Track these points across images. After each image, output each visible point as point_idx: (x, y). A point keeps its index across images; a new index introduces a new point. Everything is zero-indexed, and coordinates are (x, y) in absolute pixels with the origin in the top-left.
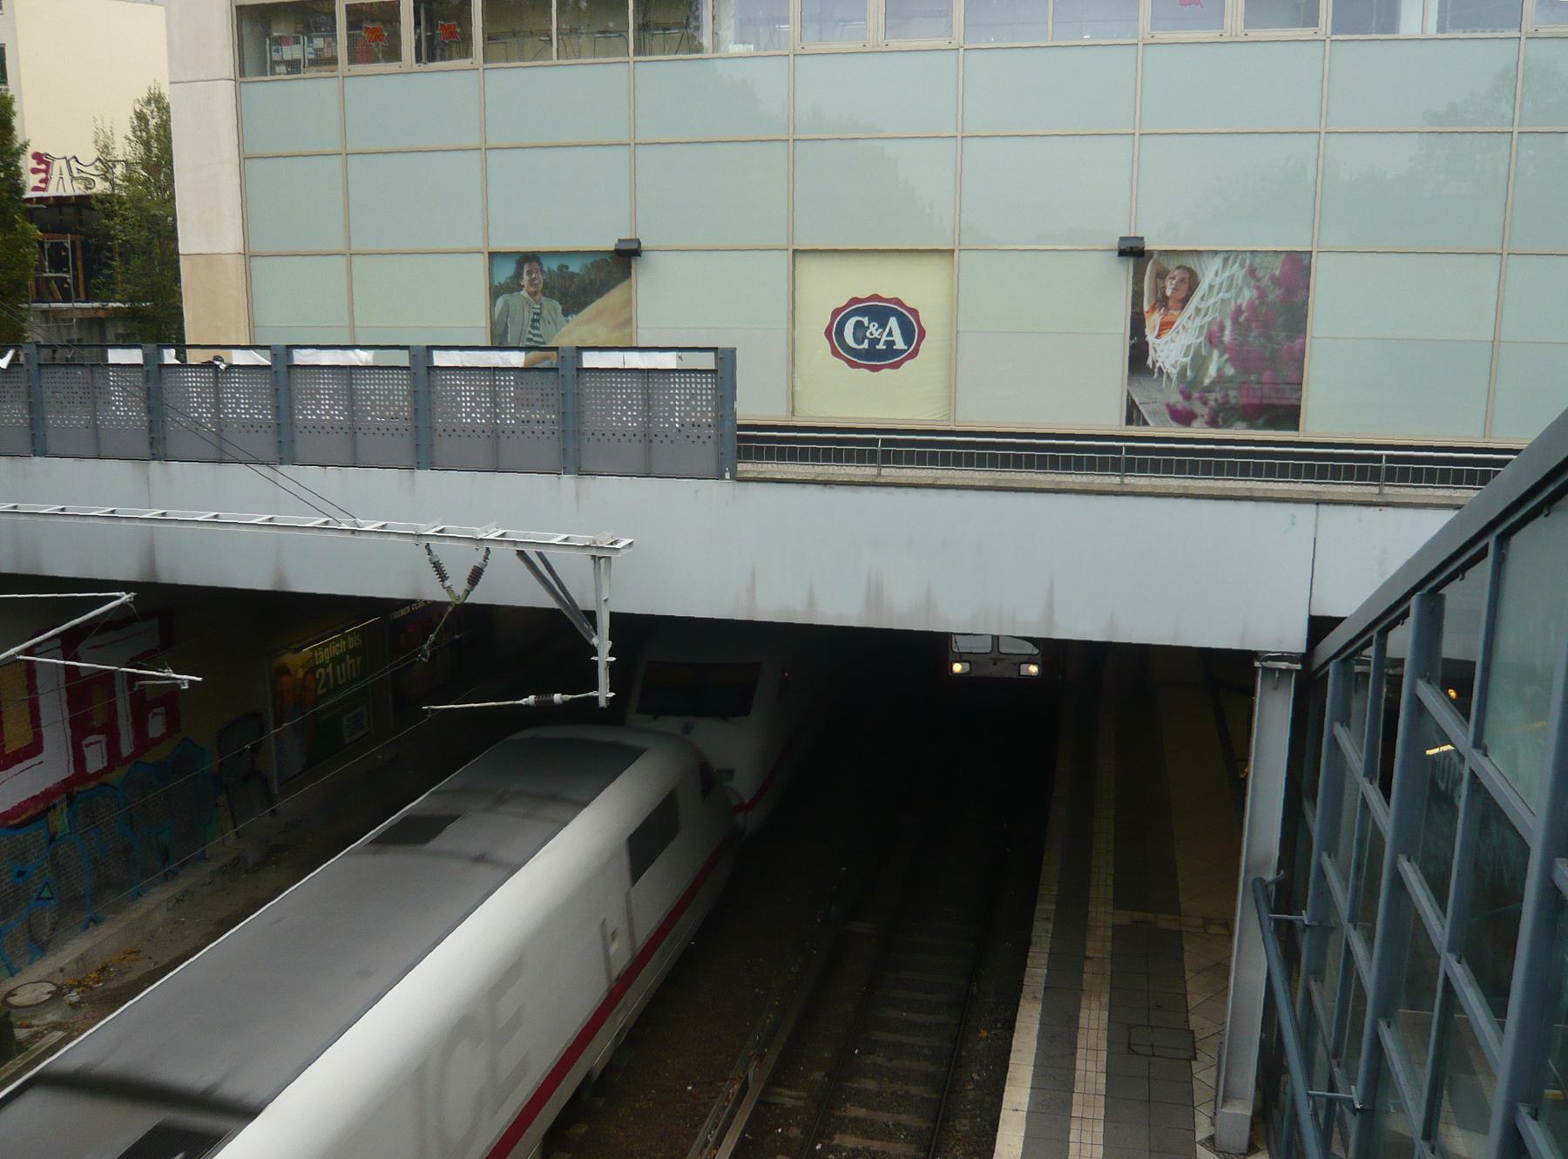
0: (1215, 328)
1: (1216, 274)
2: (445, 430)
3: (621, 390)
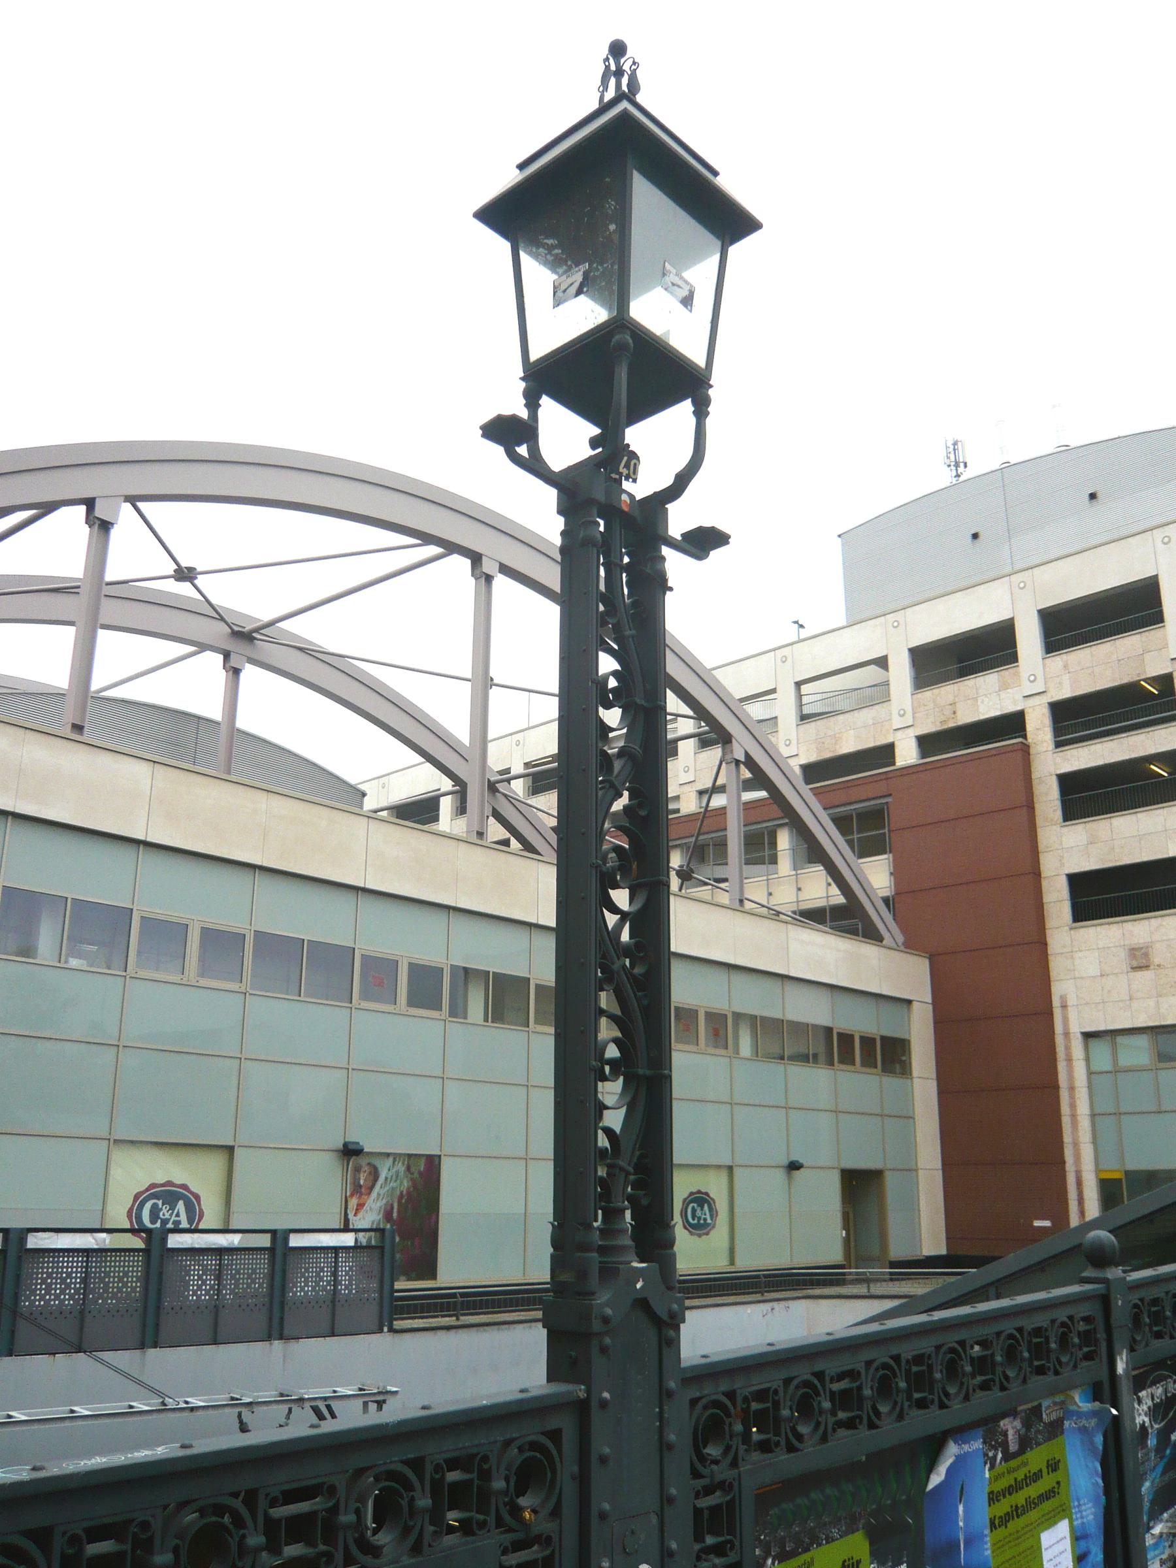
0: (389, 1208)
1: (389, 1170)
2: (172, 1309)
3: (43, 1270)
